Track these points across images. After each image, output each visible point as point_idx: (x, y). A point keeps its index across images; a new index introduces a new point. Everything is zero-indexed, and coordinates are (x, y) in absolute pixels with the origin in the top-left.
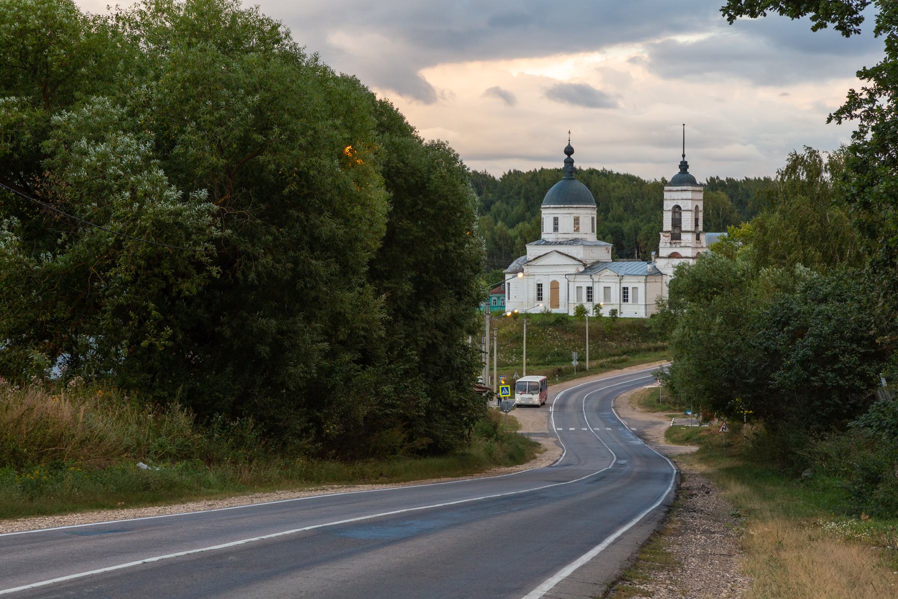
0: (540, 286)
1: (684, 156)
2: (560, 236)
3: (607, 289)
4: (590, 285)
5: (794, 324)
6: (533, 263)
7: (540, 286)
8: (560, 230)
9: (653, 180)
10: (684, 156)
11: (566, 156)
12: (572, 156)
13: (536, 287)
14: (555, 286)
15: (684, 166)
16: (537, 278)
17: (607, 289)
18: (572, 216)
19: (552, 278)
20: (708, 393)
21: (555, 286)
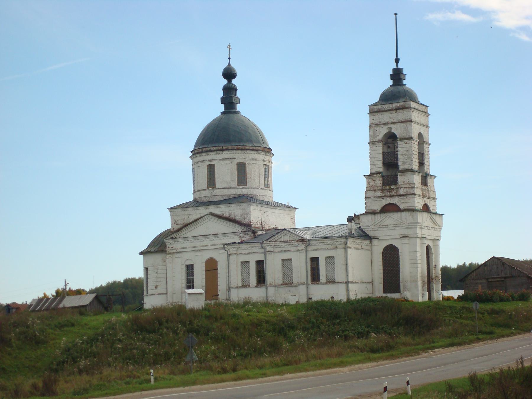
0: (190, 268)
1: (397, 61)
2: (217, 192)
3: (287, 262)
4: (260, 258)
5: (412, 185)
6: (179, 235)
7: (190, 268)
8: (218, 185)
9: (25, 303)
10: (397, 61)
11: (225, 82)
12: (234, 81)
13: (184, 269)
14: (211, 267)
15: (397, 76)
16: (187, 256)
17: (287, 262)
18: (235, 162)
19: (207, 255)
20: (406, 326)
21: (211, 267)
